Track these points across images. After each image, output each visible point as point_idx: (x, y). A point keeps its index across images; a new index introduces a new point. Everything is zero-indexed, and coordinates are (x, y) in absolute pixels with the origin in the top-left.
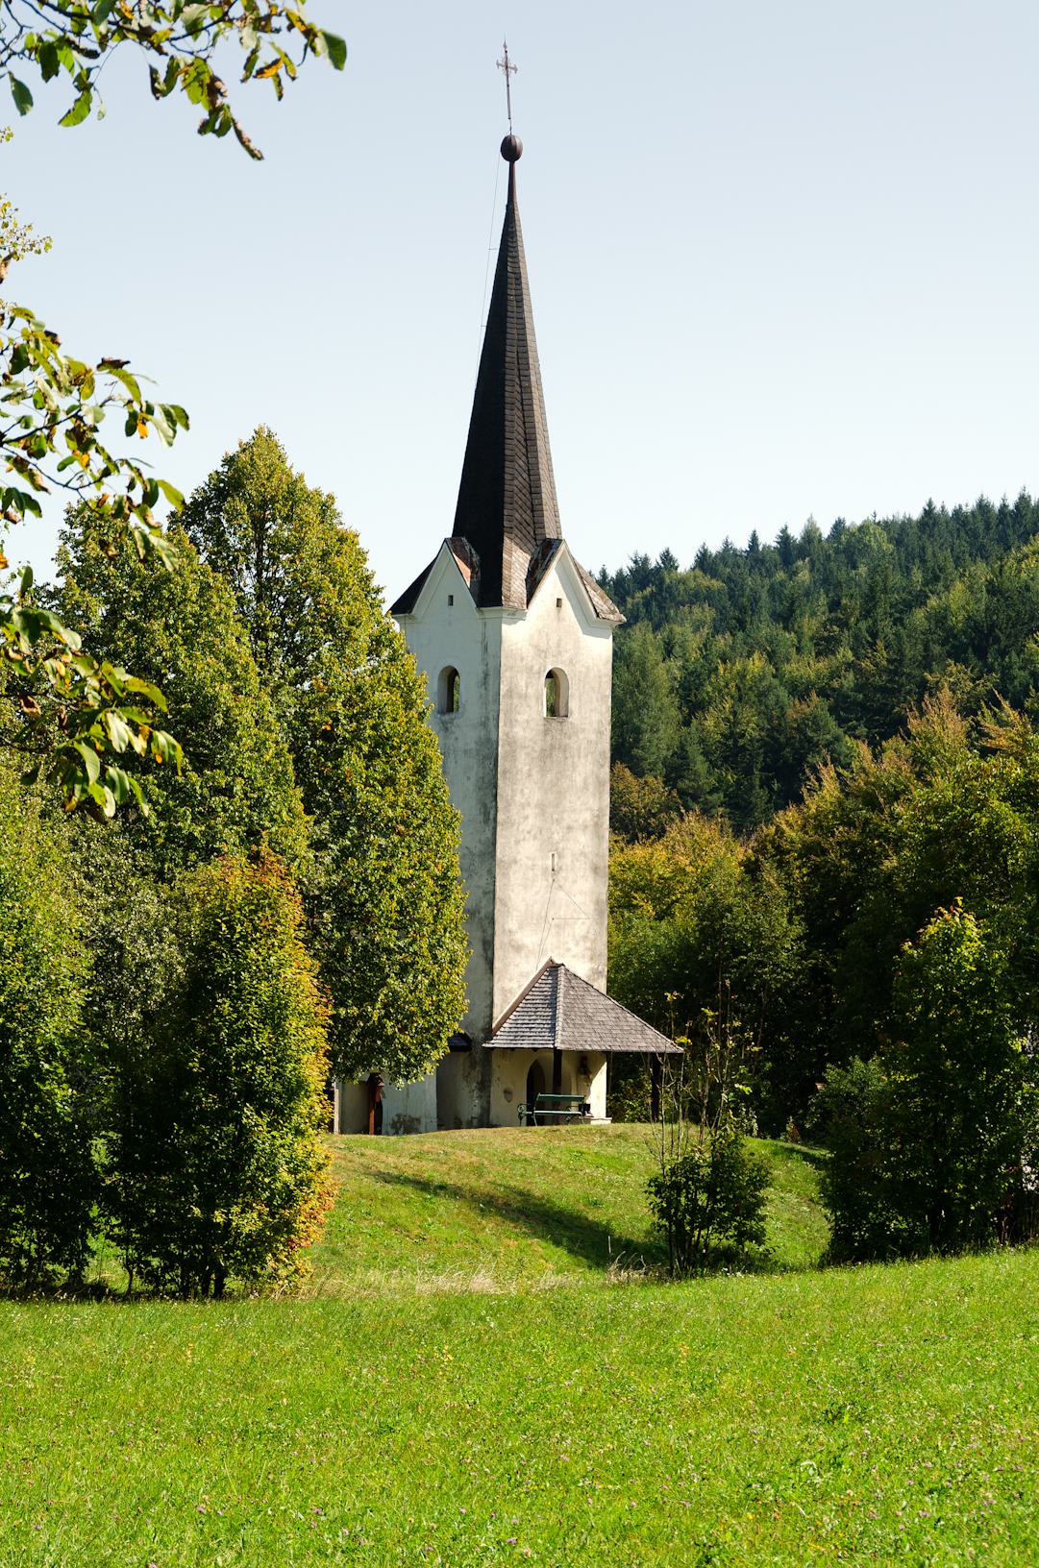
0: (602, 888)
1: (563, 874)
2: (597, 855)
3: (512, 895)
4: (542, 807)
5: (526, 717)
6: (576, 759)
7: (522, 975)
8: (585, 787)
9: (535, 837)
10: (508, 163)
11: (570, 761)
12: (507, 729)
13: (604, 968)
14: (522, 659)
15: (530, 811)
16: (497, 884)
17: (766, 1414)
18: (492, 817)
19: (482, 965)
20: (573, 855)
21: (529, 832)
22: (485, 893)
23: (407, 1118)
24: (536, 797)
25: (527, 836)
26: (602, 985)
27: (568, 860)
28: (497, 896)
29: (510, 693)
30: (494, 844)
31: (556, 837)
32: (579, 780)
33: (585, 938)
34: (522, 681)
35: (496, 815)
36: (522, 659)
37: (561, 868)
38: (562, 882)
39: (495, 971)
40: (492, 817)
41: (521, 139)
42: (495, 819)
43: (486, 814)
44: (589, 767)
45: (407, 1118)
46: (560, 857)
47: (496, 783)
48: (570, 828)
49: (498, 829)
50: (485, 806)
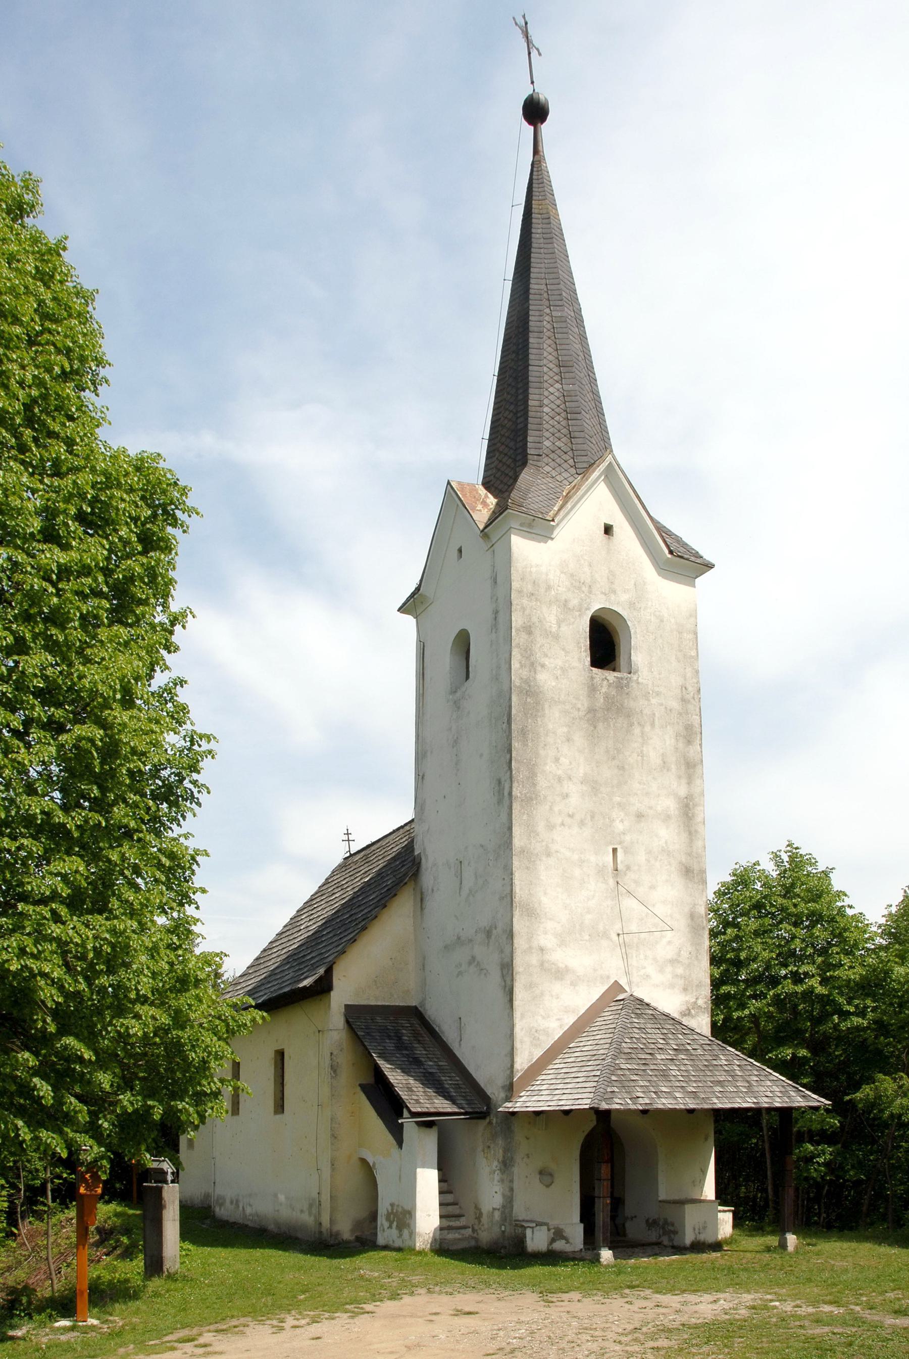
0: (708, 958)
1: (631, 875)
2: (689, 854)
3: (544, 900)
4: (593, 786)
5: (559, 663)
6: (648, 728)
7: (567, 1010)
8: (665, 766)
9: (582, 823)
10: (532, 128)
11: (637, 730)
12: (525, 673)
13: (705, 993)
14: (549, 588)
15: (573, 789)
16: (516, 882)
17: (55, 610)
18: (506, 793)
19: (508, 1006)
20: (649, 852)
21: (571, 816)
22: (502, 899)
23: (400, 1210)
24: (582, 769)
25: (568, 821)
26: (702, 1023)
27: (641, 857)
28: (516, 899)
29: (528, 630)
30: (510, 828)
31: (619, 827)
32: (654, 757)
33: (673, 962)
34: (551, 616)
35: (511, 787)
36: (549, 588)
37: (628, 868)
38: (632, 887)
39: (516, 1003)
40: (506, 793)
41: (545, 93)
42: (510, 794)
43: (500, 792)
44: (670, 741)
45: (400, 1210)
46: (626, 851)
47: (510, 745)
48: (640, 816)
49: (515, 806)
50: (499, 782)
